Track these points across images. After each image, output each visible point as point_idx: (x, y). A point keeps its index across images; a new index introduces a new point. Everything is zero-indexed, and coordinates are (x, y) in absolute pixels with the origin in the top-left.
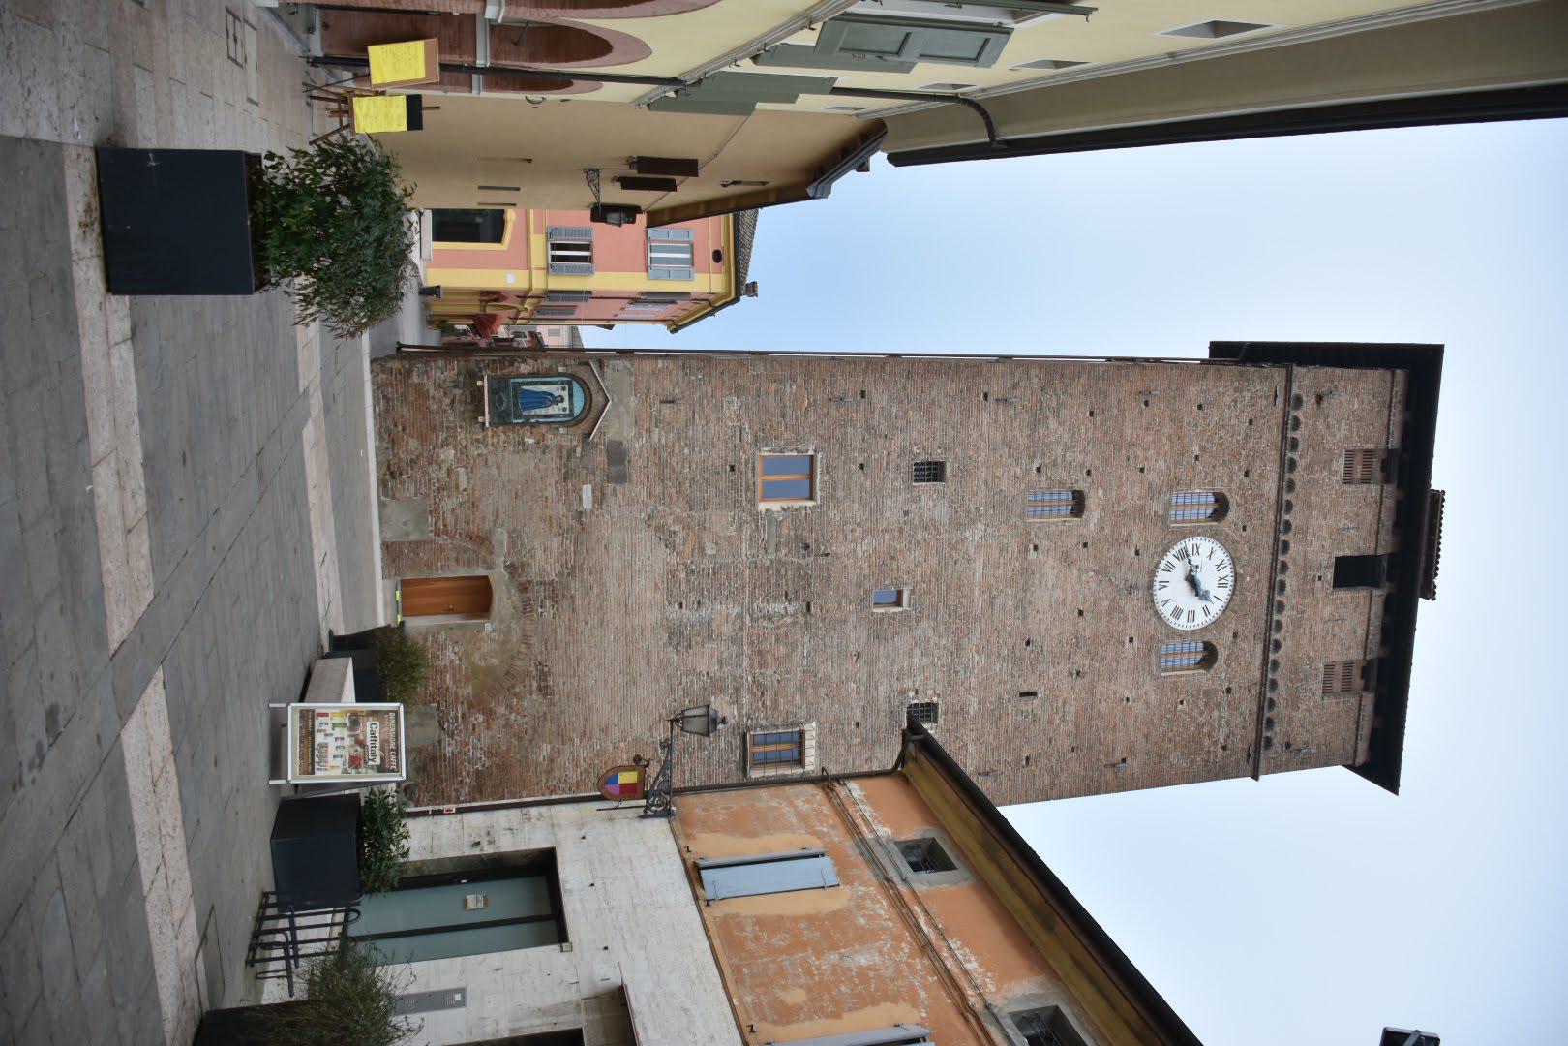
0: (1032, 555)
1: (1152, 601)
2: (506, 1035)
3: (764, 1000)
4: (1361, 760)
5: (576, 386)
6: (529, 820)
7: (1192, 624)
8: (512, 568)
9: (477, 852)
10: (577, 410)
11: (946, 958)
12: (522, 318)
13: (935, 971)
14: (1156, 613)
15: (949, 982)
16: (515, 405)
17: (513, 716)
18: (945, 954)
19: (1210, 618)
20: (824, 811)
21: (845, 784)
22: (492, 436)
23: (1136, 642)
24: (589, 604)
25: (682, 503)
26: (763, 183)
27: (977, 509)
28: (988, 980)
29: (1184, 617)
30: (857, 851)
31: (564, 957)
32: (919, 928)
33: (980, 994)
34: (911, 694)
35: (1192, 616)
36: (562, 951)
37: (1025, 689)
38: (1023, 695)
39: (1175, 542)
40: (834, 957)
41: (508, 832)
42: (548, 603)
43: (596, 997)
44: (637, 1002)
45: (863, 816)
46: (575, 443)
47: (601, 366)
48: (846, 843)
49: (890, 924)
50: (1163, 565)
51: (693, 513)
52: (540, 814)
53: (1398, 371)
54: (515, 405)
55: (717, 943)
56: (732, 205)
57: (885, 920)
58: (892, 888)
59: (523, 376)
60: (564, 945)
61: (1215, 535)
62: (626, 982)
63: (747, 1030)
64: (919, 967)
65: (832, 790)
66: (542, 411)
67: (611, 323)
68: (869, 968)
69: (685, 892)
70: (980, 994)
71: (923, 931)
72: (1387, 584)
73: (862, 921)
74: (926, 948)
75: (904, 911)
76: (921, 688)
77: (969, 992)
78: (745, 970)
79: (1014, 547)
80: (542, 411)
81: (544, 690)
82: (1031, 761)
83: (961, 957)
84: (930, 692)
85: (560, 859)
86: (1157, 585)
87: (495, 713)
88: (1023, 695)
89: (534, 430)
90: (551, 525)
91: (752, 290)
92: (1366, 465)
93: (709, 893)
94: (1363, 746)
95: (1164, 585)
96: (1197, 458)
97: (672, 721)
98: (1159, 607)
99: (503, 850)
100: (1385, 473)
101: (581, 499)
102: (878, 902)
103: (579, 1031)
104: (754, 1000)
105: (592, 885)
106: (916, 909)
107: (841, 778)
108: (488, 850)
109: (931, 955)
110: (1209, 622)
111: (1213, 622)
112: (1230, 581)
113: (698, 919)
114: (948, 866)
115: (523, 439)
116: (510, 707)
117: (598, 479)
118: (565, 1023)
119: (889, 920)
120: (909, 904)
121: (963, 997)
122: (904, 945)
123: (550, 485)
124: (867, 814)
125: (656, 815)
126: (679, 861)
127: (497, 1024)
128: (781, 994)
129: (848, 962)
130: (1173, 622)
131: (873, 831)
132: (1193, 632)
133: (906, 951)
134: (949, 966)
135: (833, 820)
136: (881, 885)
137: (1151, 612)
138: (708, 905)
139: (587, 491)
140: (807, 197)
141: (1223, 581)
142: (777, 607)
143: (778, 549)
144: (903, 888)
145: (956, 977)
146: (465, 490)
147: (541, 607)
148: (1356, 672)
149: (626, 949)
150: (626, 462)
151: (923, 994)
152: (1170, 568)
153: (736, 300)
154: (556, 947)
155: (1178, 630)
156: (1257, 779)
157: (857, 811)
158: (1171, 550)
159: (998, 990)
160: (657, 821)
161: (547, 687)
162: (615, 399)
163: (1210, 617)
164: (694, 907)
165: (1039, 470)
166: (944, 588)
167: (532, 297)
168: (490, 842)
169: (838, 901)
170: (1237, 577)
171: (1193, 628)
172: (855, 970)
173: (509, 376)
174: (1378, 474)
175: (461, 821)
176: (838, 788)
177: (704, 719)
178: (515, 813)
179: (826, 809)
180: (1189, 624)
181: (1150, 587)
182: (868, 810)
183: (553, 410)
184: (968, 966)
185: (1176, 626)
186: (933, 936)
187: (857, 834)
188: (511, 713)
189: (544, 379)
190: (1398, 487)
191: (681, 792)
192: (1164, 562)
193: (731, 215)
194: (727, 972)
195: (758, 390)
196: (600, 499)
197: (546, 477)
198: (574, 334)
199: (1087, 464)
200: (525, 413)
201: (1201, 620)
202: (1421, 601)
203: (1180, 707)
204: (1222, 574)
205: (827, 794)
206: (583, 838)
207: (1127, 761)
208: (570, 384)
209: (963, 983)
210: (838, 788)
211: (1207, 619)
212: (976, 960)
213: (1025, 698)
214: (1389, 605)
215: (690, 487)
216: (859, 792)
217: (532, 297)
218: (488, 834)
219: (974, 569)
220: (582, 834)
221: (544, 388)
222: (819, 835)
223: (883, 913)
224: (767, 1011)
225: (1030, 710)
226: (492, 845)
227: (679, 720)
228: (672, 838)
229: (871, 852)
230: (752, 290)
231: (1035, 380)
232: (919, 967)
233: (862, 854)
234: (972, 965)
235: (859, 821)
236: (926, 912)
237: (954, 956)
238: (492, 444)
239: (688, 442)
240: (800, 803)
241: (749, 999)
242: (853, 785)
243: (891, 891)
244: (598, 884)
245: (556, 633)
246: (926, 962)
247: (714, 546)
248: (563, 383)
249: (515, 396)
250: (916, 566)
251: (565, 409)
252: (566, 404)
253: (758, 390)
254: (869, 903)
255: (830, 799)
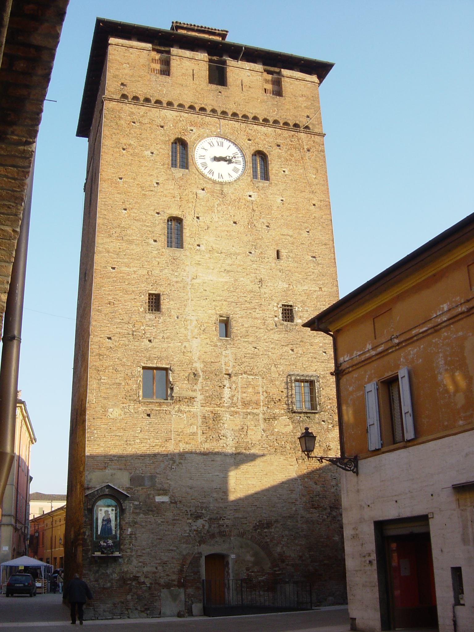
8: (202, 541)
9: (375, 562)
11: (441, 320)
15: (454, 319)
18: (439, 320)
20: (356, 376)
26: (193, 485)
34: (276, 319)
41: (364, 546)
46: (131, 505)
47: (88, 488)
50: (210, 176)
53: (109, 42)
59: (92, 534)
64: (446, 334)
65: (344, 370)
74: (436, 329)
77: (460, 310)
78: (446, 423)
83: (441, 312)
86: (221, 180)
88: (278, 257)
89: (124, 528)
95: (220, 176)
97: (309, 457)
98: (232, 179)
99: (374, 548)
105: (396, 502)
106: (414, 332)
112: (220, 140)
115: (128, 535)
123: (155, 520)
125: (356, 466)
134: (446, 319)
135: (361, 371)
139: (158, 499)
141: (220, 144)
143: (195, 391)
145: (452, 316)
149: (433, 485)
150: (143, 475)
152: (211, 172)
160: (359, 465)
165: (155, 241)
170: (218, 136)
177: (307, 438)
179: (355, 375)
181: (221, 184)
182: (356, 353)
186: (430, 325)
190: (172, 47)
196: (164, 492)
203: (286, 173)
204: (216, 144)
205: (346, 374)
206: (369, 506)
209: (454, 312)
214: (235, 57)
220: (366, 507)
224: (468, 414)
225: (286, 254)
232: (446, 334)
235: (363, 358)
242: (341, 360)
244: (396, 498)
251: (112, 510)
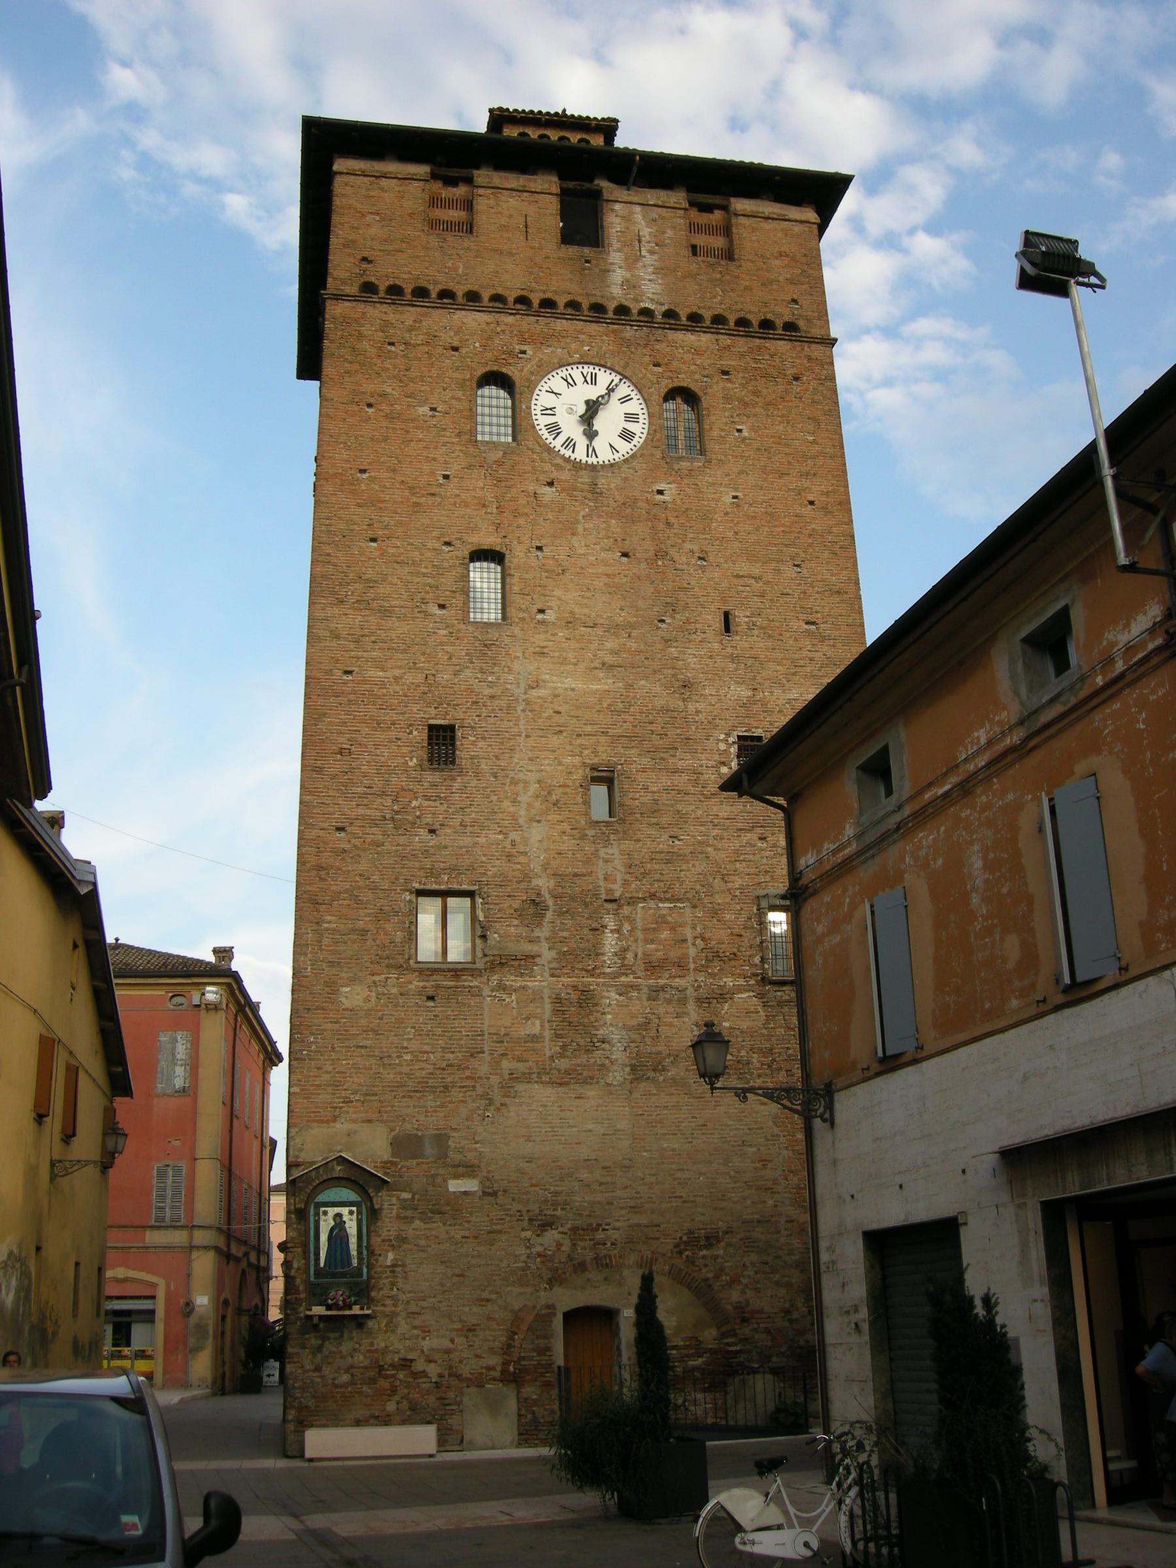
0: (550, 616)
1: (612, 465)
2: (1046, 1290)
3: (1017, 984)
4: (811, 215)
5: (321, 1198)
6: (834, 1262)
7: (641, 417)
8: (556, 1280)
9: (865, 1327)
10: (352, 1196)
12: (259, 1261)
13: (987, 780)
14: (626, 461)
15: (1000, 762)
16: (343, 1275)
17: (745, 1281)
18: (971, 767)
19: (634, 395)
21: (801, 872)
22: (384, 1305)
23: (661, 487)
24: (601, 1184)
25: (474, 1063)
27: (491, 685)
28: (997, 718)
29: (631, 427)
30: (870, 862)
31: (972, 1221)
32: (946, 795)
33: (1011, 729)
35: (631, 417)
36: (965, 1224)
37: (718, 624)
38: (727, 629)
39: (538, 438)
40: (975, 899)
41: (846, 1288)
42: (600, 1235)
43: (1011, 1182)
44: (1016, 1136)
45: (835, 852)
46: (394, 1200)
48: (861, 875)
49: (943, 829)
50: (567, 453)
51: (486, 1049)
52: (829, 1249)
54: (343, 1275)
55: (962, 1037)
56: (103, 985)
57: (939, 835)
58: (907, 823)
59: (308, 1264)
60: (960, 1221)
61: (531, 387)
62: (997, 1149)
63: (1043, 1008)
65: (807, 887)
66: (353, 1241)
67: (267, 1143)
68: (985, 858)
69: (907, 1075)
70: (1011, 729)
71: (950, 790)
72: (596, 182)
73: (940, 862)
74: (965, 789)
75: (931, 810)
76: (716, 757)
78: (987, 1006)
79: (540, 639)
80: (353, 1241)
81: (711, 1240)
82: (811, 618)
83: (975, 748)
84: (722, 746)
85: (874, 1226)
86: (592, 460)
87: (739, 1302)
88: (727, 629)
90: (500, 1232)
91: (224, 953)
92: (449, 204)
93: (908, 1046)
94: (794, 212)
96: (433, 409)
100: (460, 184)
101: (465, 1193)
102: (920, 842)
103: (1043, 1203)
104: (1016, 998)
105: (901, 1186)
106: (928, 796)
107: (794, 875)
108: (864, 1313)
109: (971, 784)
110: (639, 396)
111: (640, 391)
112: (588, 369)
113: (936, 1059)
114: (884, 752)
115: (389, 1267)
116: (734, 1281)
117: (441, 1171)
118: (1034, 1219)
119: (938, 832)
120: (922, 805)
121: (1012, 749)
122: (963, 815)
124: (832, 847)
125: (830, 1107)
126: (879, 1081)
127: (1035, 1301)
128: (1011, 965)
129: (979, 882)
130: (638, 441)
131: (849, 842)
132: (650, 415)
133: (969, 812)
136: (904, 836)
137: (625, 468)
138: (922, 1048)
140: (94, 895)
141: (589, 379)
142: (610, 942)
144: (907, 811)
146: (452, 1341)
147: (605, 1244)
148: (704, 218)
151: (1010, 797)
153: (236, 976)
154: (962, 1230)
155: (648, 434)
156: (836, 340)
157: (828, 860)
158: (548, 442)
159: (1005, 708)
161: (707, 1238)
162: (339, 1148)
163: (633, 395)
164: (925, 1064)
165: (442, 607)
166: (589, 728)
167: (228, 1245)
168: (856, 1311)
169: (917, 884)
171: (646, 416)
172: (987, 876)
173: (307, 1282)
174: (461, 191)
175: (834, 1345)
176: (804, 881)
178: (825, 1279)
180: (641, 420)
181: (593, 468)
182: (829, 846)
183: (351, 1227)
184: (983, 741)
185: (644, 436)
186: (954, 780)
187: (852, 861)
188: (740, 1282)
189: (312, 1238)
191: (806, 1076)
192: (563, 451)
193: (115, 981)
194: (988, 1027)
195: (332, 964)
196: (468, 1169)
197: (436, 1237)
198: (278, 1189)
199: (437, 545)
200: (355, 1262)
201: (636, 406)
202: (620, 142)
203: (745, 433)
204: (579, 379)
205: (811, 895)
206: (853, 1196)
207: (811, 499)
208: (318, 1205)
209: (999, 748)
210: (804, 881)
211: (635, 398)
212: (977, 731)
213: (731, 627)
215: (453, 1053)
216: (809, 855)
217: (228, 1245)
218: (848, 1312)
219: (566, 689)
221: (324, 1238)
222: (854, 906)
223: (931, 837)
226: (860, 1309)
227: (710, 1076)
228: (855, 1088)
229: (868, 848)
230: (224, 953)
231: (329, 612)
233: (873, 857)
234: (982, 736)
235: (840, 857)
236: (930, 785)
237: (974, 756)
238: (394, 1305)
239: (394, 1055)
240: (820, 929)
241: (1014, 1003)
242: (802, 863)
243: (910, 825)
244: (898, 1179)
245: (639, 1225)
246: (979, 790)
247: (529, 1022)
248: (317, 1214)
249: (334, 1275)
250: (560, 763)
251: (351, 1213)
252: (345, 1211)
253: (332, 964)
254: (922, 853)
255: (815, 893)
